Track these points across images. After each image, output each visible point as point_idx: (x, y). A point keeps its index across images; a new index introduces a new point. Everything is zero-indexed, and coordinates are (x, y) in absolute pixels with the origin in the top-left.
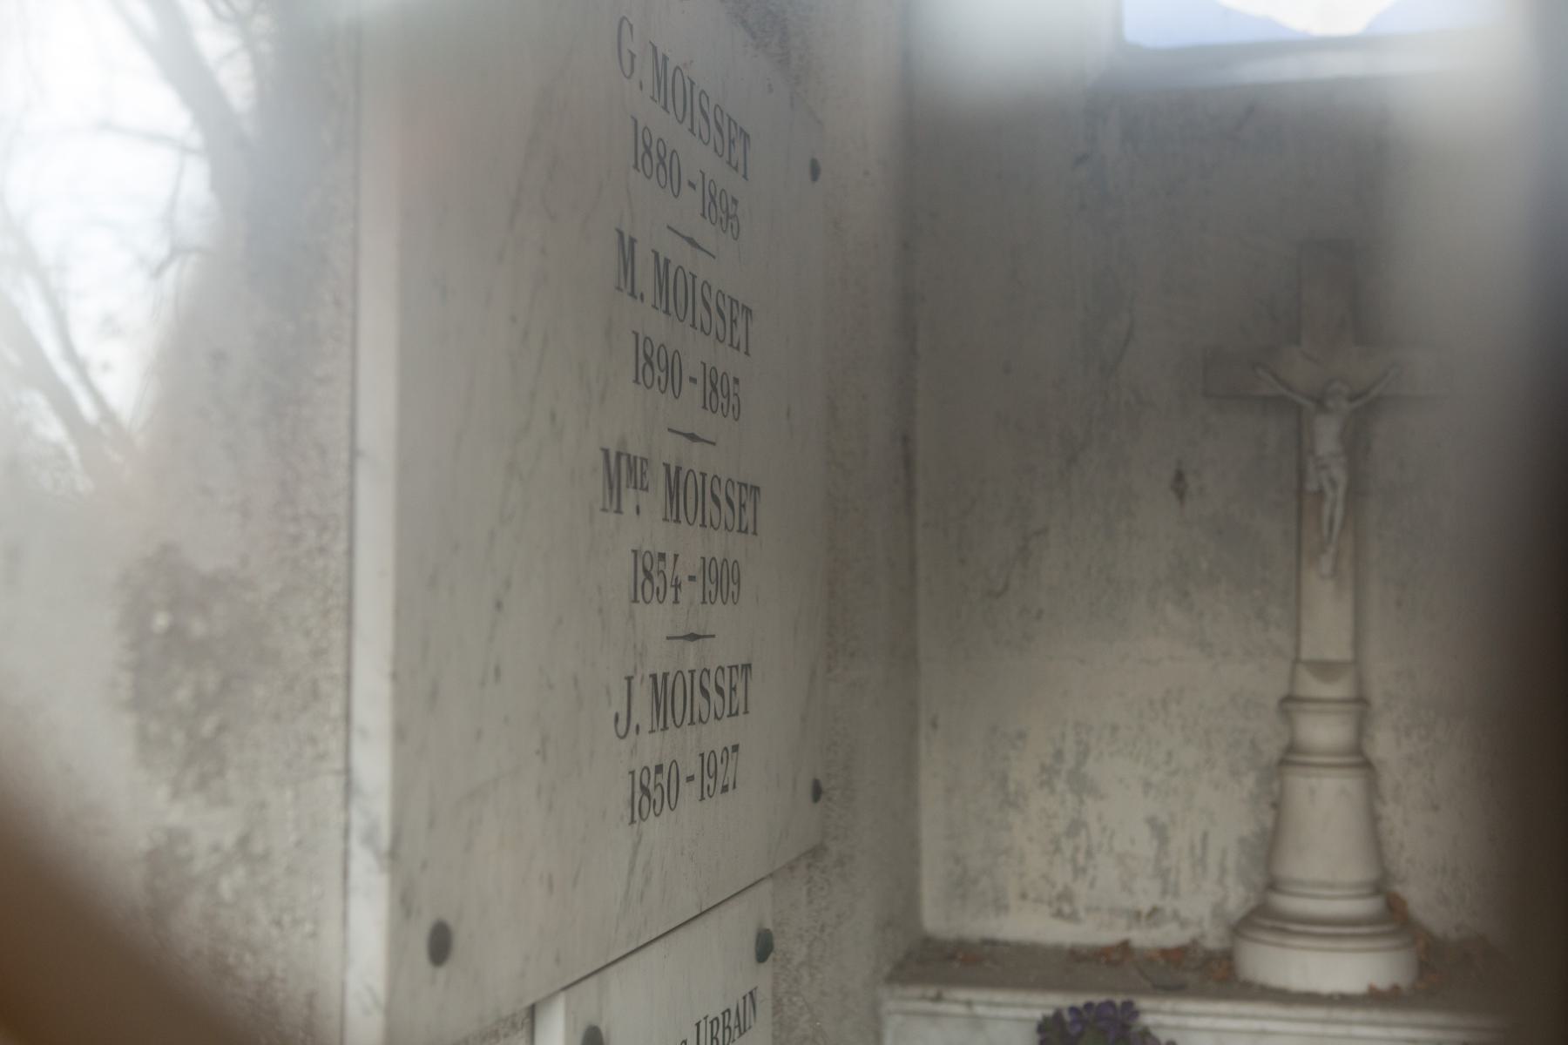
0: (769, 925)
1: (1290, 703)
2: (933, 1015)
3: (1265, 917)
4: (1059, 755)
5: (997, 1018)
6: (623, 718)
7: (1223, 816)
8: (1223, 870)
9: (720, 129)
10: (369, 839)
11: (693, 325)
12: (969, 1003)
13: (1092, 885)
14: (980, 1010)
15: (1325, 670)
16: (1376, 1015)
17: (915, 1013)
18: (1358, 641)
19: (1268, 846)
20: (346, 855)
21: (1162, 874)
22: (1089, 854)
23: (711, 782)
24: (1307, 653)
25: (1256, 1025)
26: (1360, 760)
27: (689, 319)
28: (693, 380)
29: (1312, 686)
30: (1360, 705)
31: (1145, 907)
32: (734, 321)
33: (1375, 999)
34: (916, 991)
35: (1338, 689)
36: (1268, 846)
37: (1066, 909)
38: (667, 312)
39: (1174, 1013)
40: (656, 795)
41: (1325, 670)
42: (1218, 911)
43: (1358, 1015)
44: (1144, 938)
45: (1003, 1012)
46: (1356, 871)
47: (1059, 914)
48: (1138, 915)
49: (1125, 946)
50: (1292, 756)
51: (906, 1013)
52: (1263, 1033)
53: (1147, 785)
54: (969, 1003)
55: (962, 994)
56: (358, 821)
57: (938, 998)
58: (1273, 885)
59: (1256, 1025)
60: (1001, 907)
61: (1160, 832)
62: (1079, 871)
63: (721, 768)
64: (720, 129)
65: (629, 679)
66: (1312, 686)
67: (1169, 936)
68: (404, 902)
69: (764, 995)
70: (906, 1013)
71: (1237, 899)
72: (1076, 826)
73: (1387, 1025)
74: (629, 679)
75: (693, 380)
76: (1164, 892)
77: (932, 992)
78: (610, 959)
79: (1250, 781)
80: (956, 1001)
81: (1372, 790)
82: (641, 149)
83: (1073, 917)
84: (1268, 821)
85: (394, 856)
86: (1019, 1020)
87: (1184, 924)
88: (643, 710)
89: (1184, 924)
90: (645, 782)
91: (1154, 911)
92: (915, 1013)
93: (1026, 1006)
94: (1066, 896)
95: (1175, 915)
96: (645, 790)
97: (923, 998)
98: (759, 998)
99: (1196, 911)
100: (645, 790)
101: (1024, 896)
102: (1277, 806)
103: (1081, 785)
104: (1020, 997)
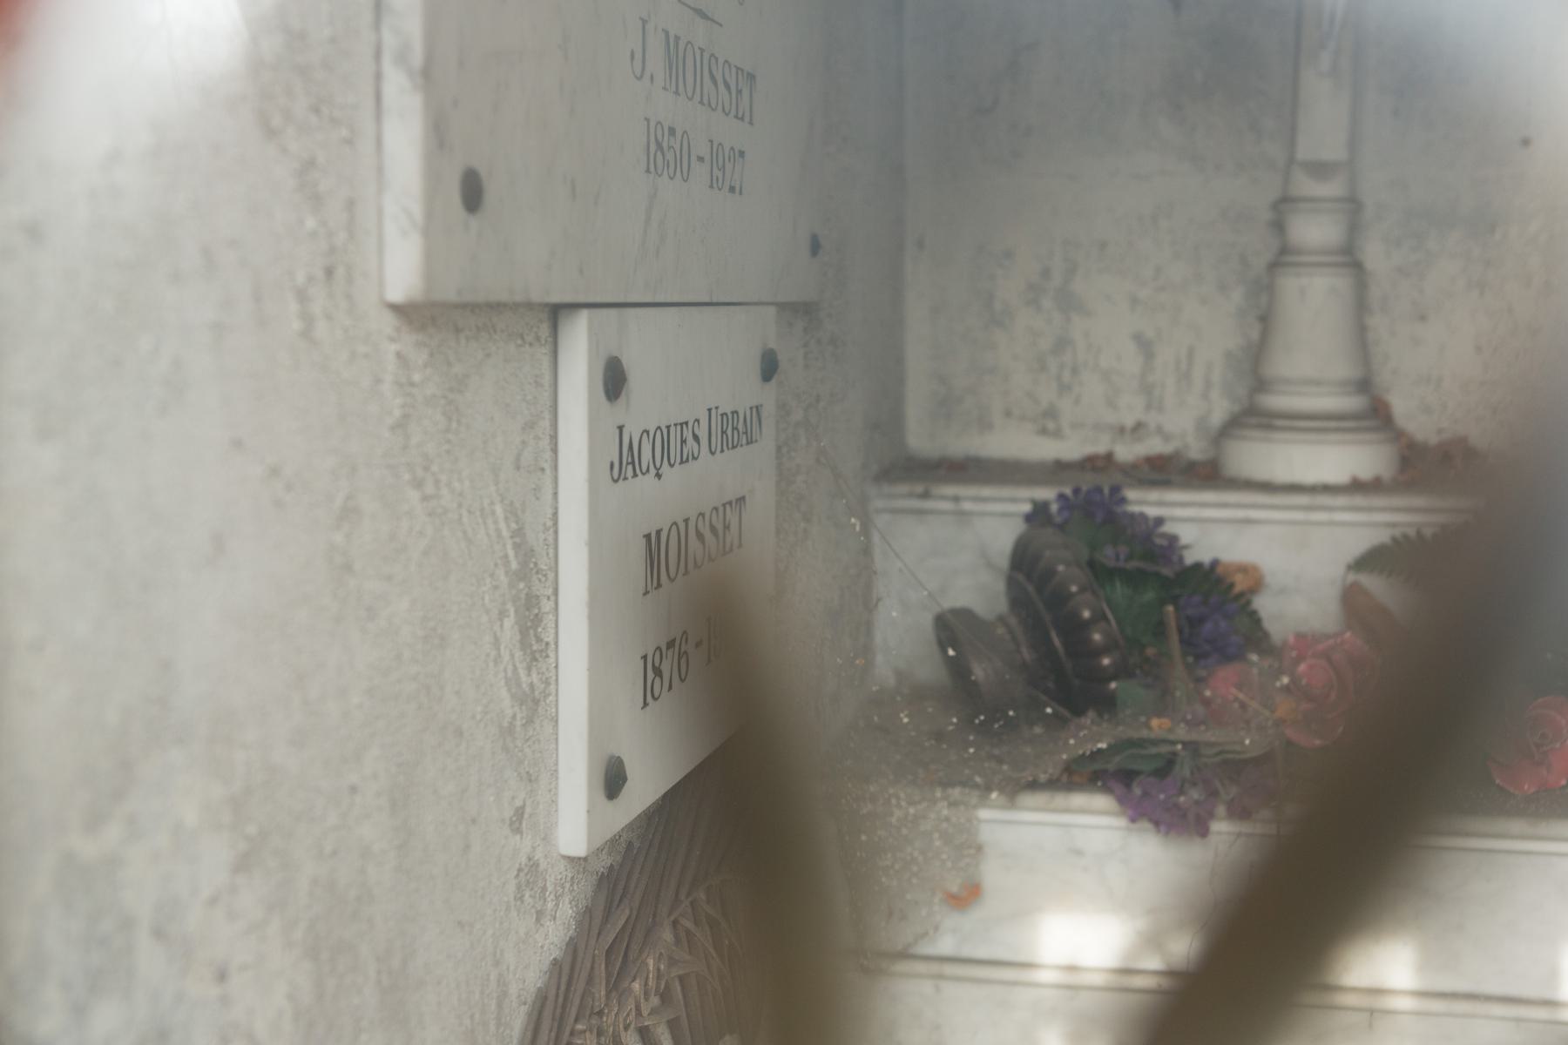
0: (772, 345)
1: (1284, 205)
2: (921, 512)
3: (1252, 417)
4: (1046, 273)
5: (983, 514)
6: (638, 56)
7: (1210, 331)
8: (1208, 384)
9: (727, 86)
10: (401, 58)
11: (701, 102)
12: (956, 499)
13: (1077, 401)
14: (967, 506)
15: (1320, 170)
16: (1359, 500)
17: (903, 511)
18: (1353, 143)
19: (1253, 366)
20: (378, 77)
21: (1147, 389)
22: (1075, 371)
23: (720, 175)
24: (1302, 153)
25: (1240, 514)
26: (1349, 259)
27: (697, 98)
28: (701, 159)
29: (1306, 186)
30: (1352, 206)
31: (1129, 422)
32: (739, 92)
33: (1356, 486)
34: (903, 488)
35: (1332, 188)
36: (1253, 366)
37: (1051, 425)
38: (677, 93)
39: (1160, 504)
40: (670, 156)
41: (1320, 170)
42: (1201, 424)
43: (1341, 500)
44: (1126, 452)
45: (991, 507)
46: (1343, 369)
47: (1043, 431)
48: (1122, 430)
49: (1109, 457)
50: (1284, 257)
51: (895, 511)
52: (1248, 521)
53: (1134, 301)
54: (956, 499)
55: (950, 490)
56: (389, 40)
57: (926, 495)
58: (1261, 384)
59: (1240, 514)
60: (985, 425)
61: (1146, 347)
62: (1064, 388)
63: (729, 166)
64: (727, 86)
65: (644, 22)
66: (1306, 186)
67: (1154, 446)
68: (438, 135)
69: (769, 410)
70: (895, 511)
71: (1220, 411)
72: (1062, 344)
73: (1370, 509)
74: (644, 22)
75: (701, 159)
76: (1148, 407)
77: (919, 489)
78: (630, 300)
79: (1237, 295)
80: (943, 498)
81: (1361, 306)
82: (653, 147)
83: (1057, 434)
84: (1255, 334)
85: (427, 77)
86: (1004, 515)
87: (1167, 438)
88: (656, 64)
89: (1167, 438)
90: (658, 680)
91: (1139, 426)
92: (903, 511)
93: (1014, 500)
94: (1051, 413)
95: (1160, 430)
96: (659, 146)
97: (911, 495)
98: (764, 414)
99: (1181, 425)
100: (659, 146)
101: (1008, 414)
102: (1266, 320)
103: (1069, 303)
104: (1006, 492)
